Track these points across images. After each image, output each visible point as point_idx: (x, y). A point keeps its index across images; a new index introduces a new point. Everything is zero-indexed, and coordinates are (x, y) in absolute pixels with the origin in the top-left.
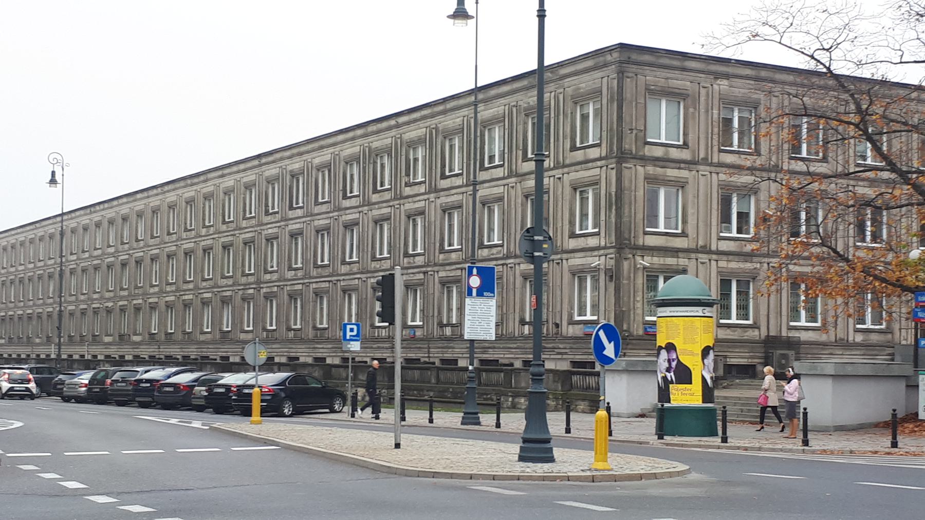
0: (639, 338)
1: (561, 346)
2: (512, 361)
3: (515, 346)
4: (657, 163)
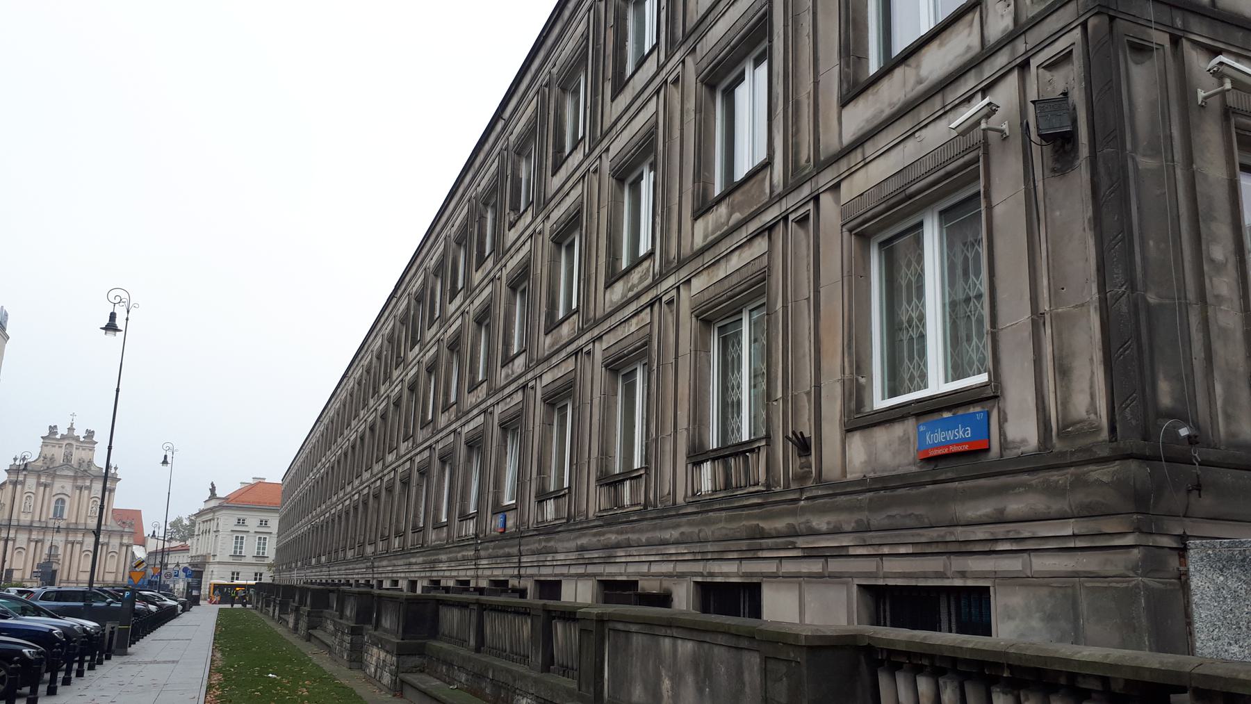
1: (820, 523)
2: (667, 583)
3: (674, 534)
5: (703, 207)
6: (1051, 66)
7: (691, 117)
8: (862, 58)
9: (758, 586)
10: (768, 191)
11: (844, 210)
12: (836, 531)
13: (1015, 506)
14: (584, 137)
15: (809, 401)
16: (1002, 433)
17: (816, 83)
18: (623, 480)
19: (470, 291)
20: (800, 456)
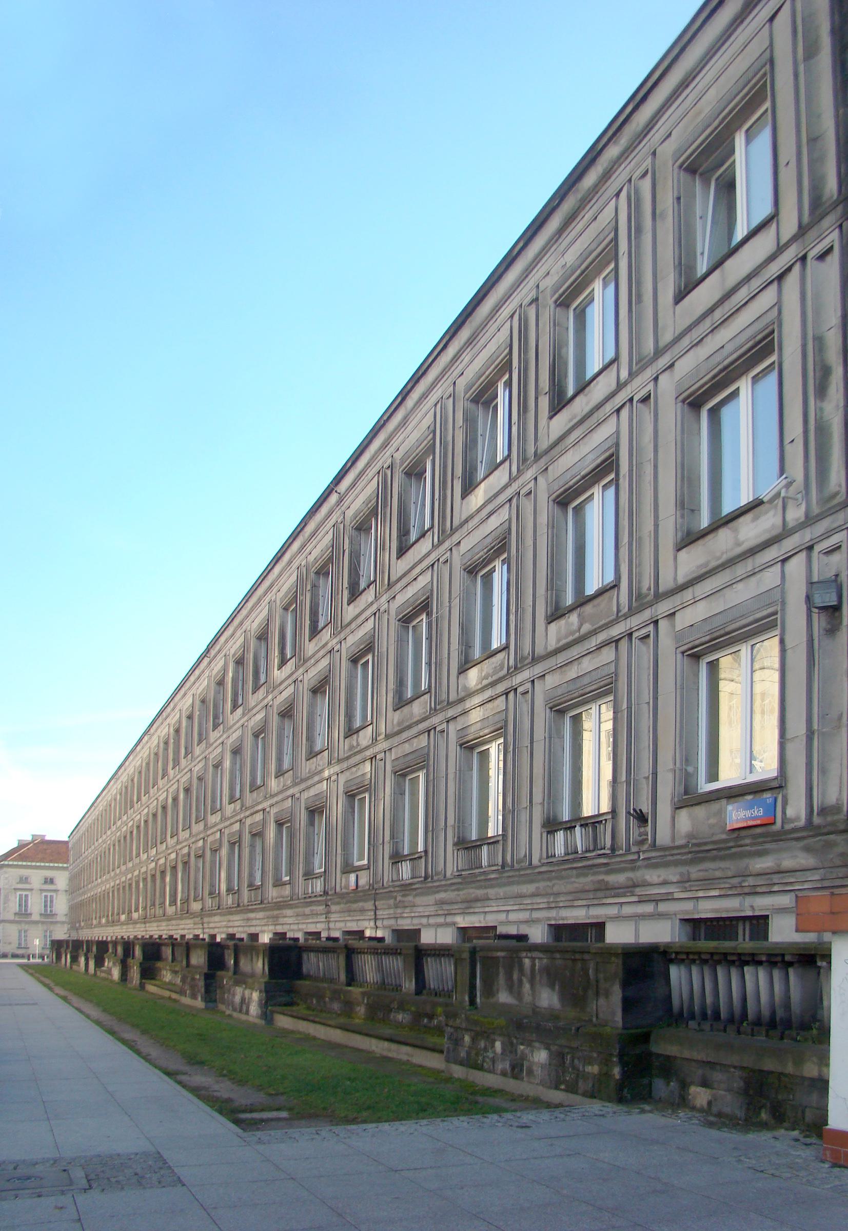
5: (556, 614)
6: (830, 552)
7: (543, 530)
8: (695, 511)
9: (419, 930)
10: (615, 609)
11: (678, 637)
12: (665, 883)
13: (788, 863)
14: (432, 527)
15: (648, 784)
16: (784, 813)
17: (656, 526)
18: (481, 845)
19: (340, 628)
20: (639, 827)
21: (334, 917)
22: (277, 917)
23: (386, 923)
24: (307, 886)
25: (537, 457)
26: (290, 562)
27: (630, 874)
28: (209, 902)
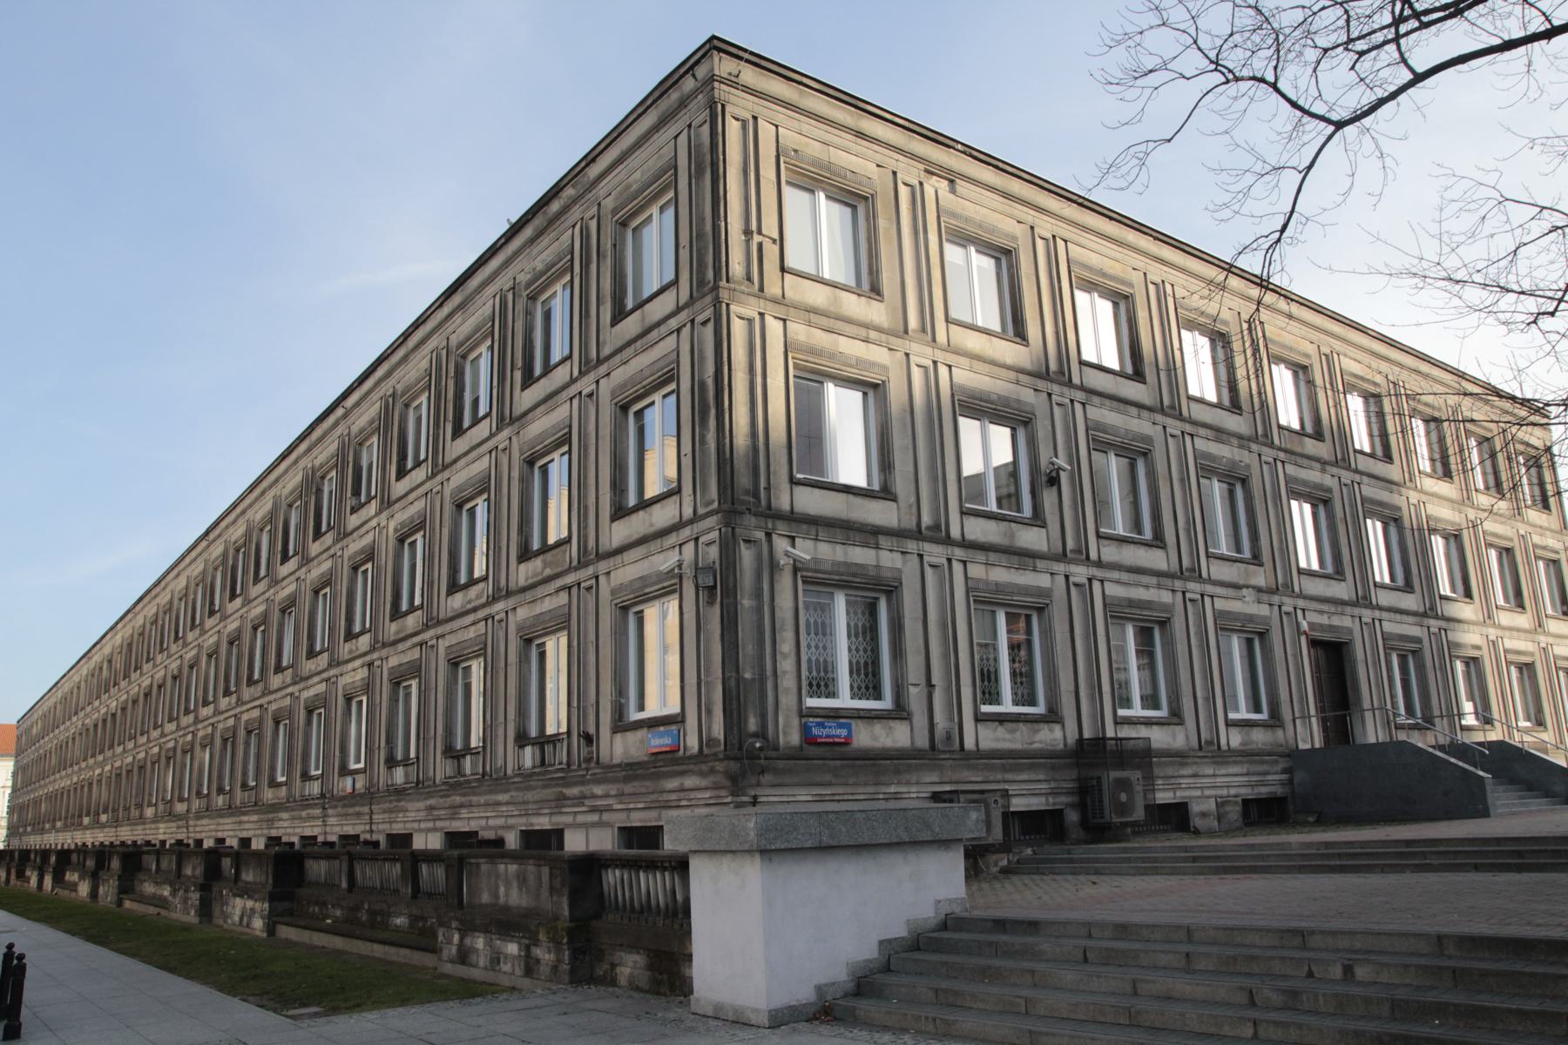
0: (795, 755)
4: (813, 317)
9: (411, 835)
11: (614, 592)
12: (607, 796)
14: (426, 459)
21: (332, 820)
22: (272, 820)
23: (381, 827)
24: (303, 789)
25: (513, 421)
26: (296, 462)
27: (582, 788)
28: (239, 795)
